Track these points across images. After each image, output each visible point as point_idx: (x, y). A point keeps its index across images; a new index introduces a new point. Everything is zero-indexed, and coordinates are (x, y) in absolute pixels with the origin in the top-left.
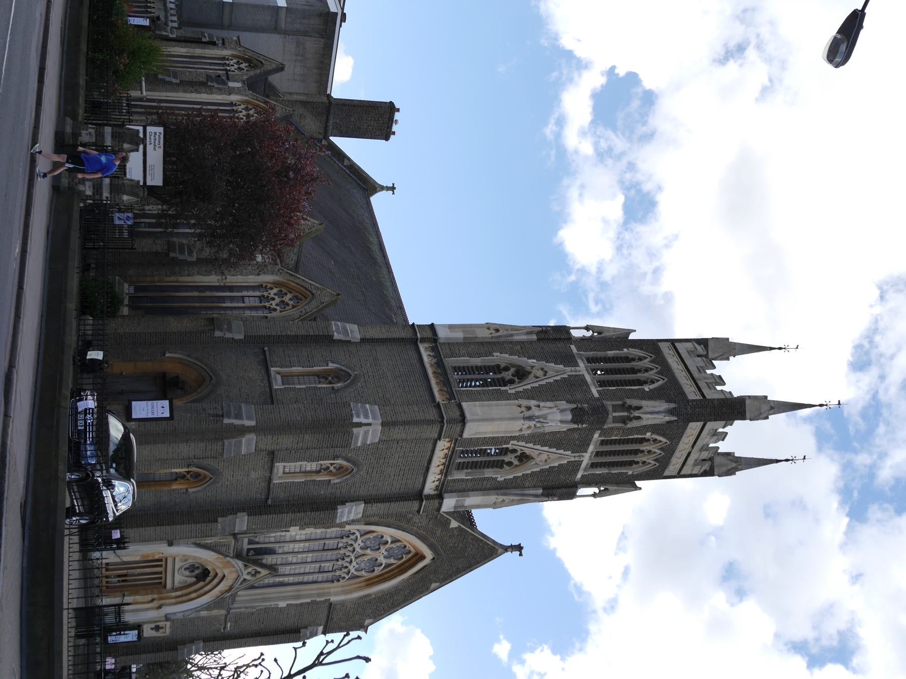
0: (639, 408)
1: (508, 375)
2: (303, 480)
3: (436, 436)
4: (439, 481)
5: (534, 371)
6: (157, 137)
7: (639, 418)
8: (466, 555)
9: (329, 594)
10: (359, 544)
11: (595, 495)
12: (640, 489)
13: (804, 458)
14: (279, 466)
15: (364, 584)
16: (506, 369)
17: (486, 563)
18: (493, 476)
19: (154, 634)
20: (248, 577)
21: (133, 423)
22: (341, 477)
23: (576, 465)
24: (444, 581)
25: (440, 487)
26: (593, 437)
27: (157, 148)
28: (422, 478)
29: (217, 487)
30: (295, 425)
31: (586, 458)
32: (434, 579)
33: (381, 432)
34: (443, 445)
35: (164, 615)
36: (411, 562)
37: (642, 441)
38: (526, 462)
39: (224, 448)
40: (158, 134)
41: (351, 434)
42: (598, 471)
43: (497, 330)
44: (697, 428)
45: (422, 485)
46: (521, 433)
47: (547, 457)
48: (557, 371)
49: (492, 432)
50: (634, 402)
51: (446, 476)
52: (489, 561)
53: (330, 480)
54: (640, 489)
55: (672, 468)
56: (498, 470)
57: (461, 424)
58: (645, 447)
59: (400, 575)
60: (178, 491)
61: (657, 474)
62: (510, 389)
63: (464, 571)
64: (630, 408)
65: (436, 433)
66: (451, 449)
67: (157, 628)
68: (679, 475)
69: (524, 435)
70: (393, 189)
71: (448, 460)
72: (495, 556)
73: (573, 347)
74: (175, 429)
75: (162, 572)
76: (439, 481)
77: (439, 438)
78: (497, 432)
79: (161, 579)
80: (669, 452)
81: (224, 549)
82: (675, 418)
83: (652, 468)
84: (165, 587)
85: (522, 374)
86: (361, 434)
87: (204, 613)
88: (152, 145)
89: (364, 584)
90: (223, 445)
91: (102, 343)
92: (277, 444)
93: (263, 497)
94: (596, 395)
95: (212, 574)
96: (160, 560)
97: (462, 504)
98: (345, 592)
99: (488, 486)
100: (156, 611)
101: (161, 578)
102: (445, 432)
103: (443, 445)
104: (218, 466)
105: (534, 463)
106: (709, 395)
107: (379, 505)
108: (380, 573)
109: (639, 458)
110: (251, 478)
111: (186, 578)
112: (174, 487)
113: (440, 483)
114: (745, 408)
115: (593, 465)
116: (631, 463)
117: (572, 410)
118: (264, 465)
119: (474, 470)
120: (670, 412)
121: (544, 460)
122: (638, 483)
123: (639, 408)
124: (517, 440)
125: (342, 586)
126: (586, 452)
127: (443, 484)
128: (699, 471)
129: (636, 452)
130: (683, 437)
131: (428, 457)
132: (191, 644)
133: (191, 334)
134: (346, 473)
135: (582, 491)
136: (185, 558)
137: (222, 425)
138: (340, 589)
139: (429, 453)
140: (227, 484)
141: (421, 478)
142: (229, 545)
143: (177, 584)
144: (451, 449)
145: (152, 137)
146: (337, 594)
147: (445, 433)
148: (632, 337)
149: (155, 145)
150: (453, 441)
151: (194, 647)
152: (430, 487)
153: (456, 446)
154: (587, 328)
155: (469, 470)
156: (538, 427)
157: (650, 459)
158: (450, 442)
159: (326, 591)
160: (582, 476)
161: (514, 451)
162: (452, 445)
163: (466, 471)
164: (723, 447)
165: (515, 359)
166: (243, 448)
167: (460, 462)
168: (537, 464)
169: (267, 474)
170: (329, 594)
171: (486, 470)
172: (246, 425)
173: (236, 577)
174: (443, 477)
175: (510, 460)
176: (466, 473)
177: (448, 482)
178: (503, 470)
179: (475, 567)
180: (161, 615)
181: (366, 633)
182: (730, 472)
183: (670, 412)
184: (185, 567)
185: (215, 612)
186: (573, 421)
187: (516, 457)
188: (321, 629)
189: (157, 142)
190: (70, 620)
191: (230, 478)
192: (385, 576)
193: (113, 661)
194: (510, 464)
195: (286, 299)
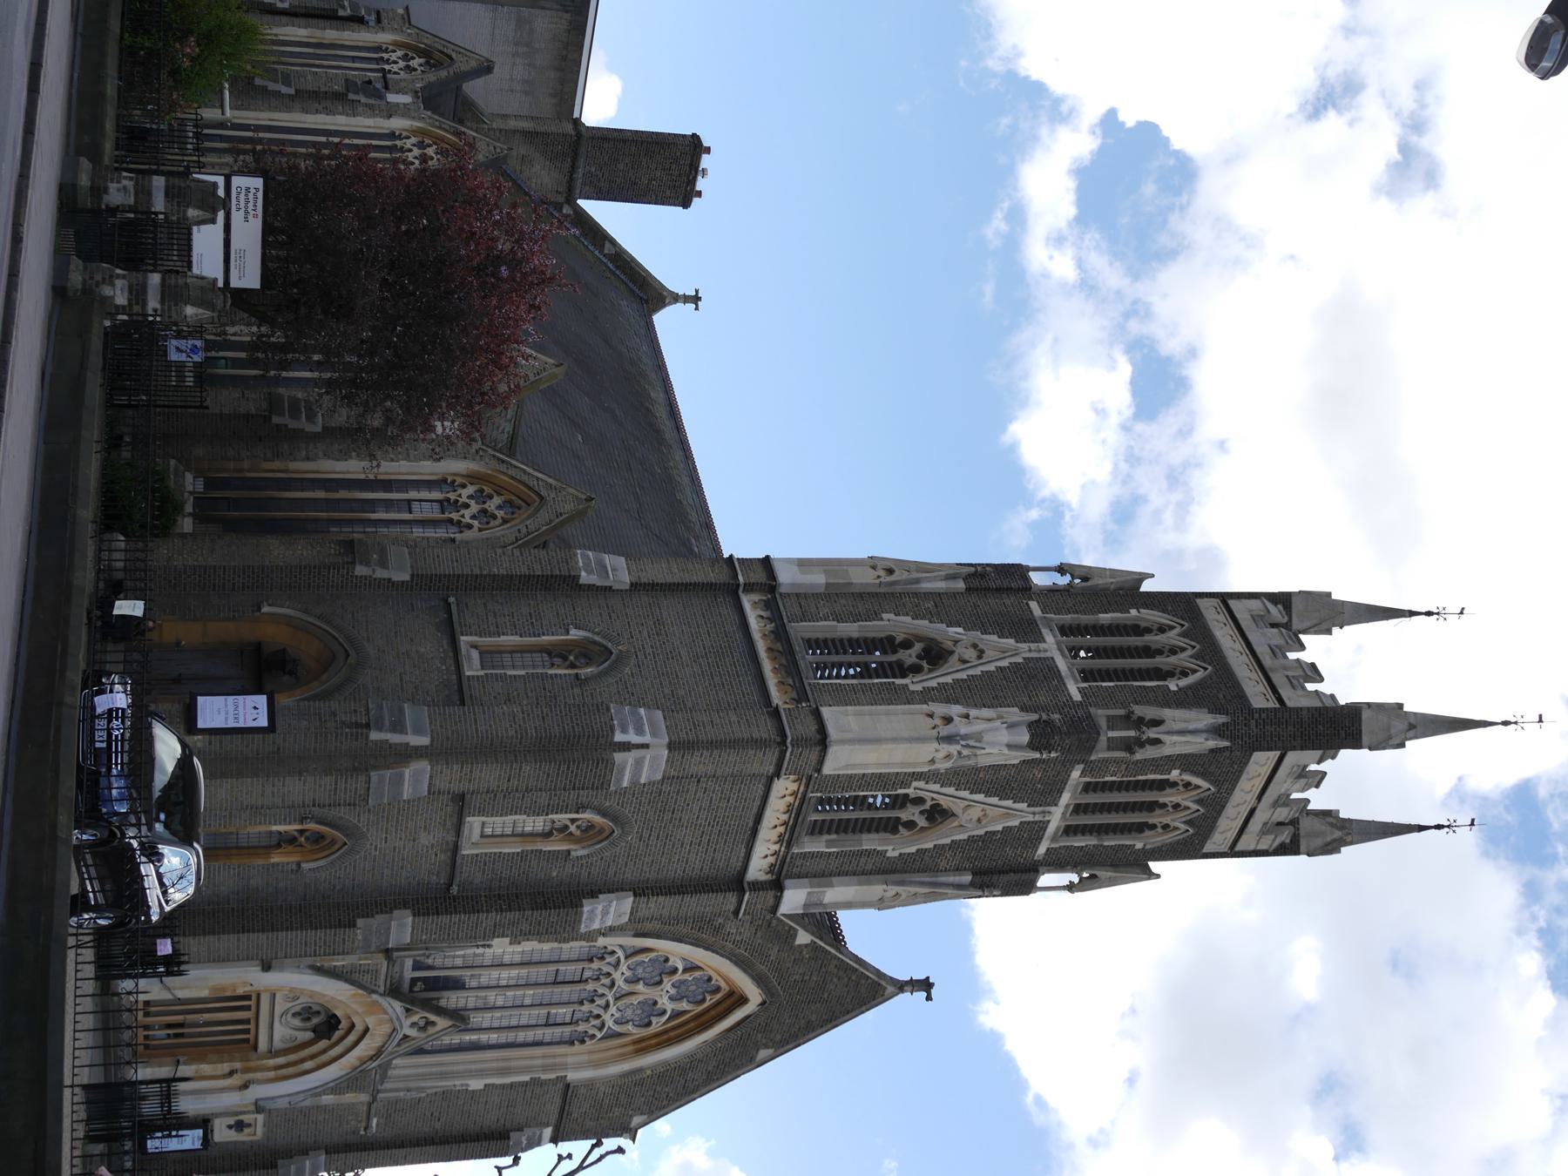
0: (1157, 723)
1: (909, 657)
3: (771, 769)
5: (959, 650)
6: (251, 196)
7: (1157, 742)
9: (565, 1067)
11: (1071, 888)
12: (1158, 876)
13: (1541, 721)
14: (474, 823)
16: (907, 644)
19: (233, 1136)
20: (413, 1033)
21: (200, 737)
23: (1035, 831)
27: (250, 218)
28: (743, 850)
31: (1056, 817)
32: (764, 1041)
33: (667, 761)
34: (784, 788)
35: (254, 1101)
36: (720, 1008)
38: (941, 823)
39: (369, 788)
40: (253, 191)
42: (1079, 842)
43: (890, 571)
44: (1269, 762)
46: (933, 767)
48: (1002, 651)
49: (879, 765)
50: (1150, 712)
53: (569, 852)
54: (1158, 876)
55: (1219, 839)
56: (888, 835)
57: (818, 748)
58: (1168, 797)
59: (699, 1032)
61: (1190, 848)
62: (914, 684)
64: (1140, 723)
65: (770, 764)
67: (240, 1126)
68: (1233, 852)
70: (695, 299)
72: (880, 1000)
73: (1034, 605)
74: (279, 749)
77: (777, 774)
78: (888, 765)
79: (250, 1000)
80: (1214, 807)
82: (1226, 744)
83: (1182, 837)
84: (255, 1048)
85: (935, 655)
86: (629, 764)
87: (327, 1099)
88: (242, 212)
94: (1077, 696)
95: (344, 1025)
98: (596, 1065)
99: (869, 867)
101: (247, 1031)
103: (784, 788)
104: (359, 821)
105: (956, 824)
106: (1292, 699)
107: (661, 899)
109: (1156, 818)
111: (293, 1032)
116: (1140, 828)
117: (1030, 725)
119: (843, 836)
120: (1218, 731)
122: (1154, 866)
123: (1157, 723)
126: (1056, 805)
127: (783, 862)
128: (1271, 846)
129: (1152, 806)
131: (755, 810)
134: (600, 838)
135: (1045, 879)
136: (294, 995)
138: (585, 1058)
139: (757, 803)
143: (277, 1044)
145: (242, 197)
146: (579, 1067)
148: (1147, 587)
149: (247, 212)
151: (308, 1162)
152: (758, 868)
153: (809, 790)
154: (1061, 569)
155: (834, 836)
159: (558, 1060)
161: (919, 801)
163: (826, 837)
164: (1318, 799)
165: (923, 626)
169: (451, 838)
170: (565, 1067)
171: (865, 836)
173: (390, 1031)
174: (783, 849)
175: (912, 818)
177: (792, 858)
178: (897, 836)
179: (841, 1020)
182: (1331, 848)
183: (1218, 731)
185: (349, 1097)
186: (1032, 746)
187: (922, 812)
188: (548, 1132)
189: (251, 205)
192: (672, 1034)
194: (910, 825)
195: (492, 505)
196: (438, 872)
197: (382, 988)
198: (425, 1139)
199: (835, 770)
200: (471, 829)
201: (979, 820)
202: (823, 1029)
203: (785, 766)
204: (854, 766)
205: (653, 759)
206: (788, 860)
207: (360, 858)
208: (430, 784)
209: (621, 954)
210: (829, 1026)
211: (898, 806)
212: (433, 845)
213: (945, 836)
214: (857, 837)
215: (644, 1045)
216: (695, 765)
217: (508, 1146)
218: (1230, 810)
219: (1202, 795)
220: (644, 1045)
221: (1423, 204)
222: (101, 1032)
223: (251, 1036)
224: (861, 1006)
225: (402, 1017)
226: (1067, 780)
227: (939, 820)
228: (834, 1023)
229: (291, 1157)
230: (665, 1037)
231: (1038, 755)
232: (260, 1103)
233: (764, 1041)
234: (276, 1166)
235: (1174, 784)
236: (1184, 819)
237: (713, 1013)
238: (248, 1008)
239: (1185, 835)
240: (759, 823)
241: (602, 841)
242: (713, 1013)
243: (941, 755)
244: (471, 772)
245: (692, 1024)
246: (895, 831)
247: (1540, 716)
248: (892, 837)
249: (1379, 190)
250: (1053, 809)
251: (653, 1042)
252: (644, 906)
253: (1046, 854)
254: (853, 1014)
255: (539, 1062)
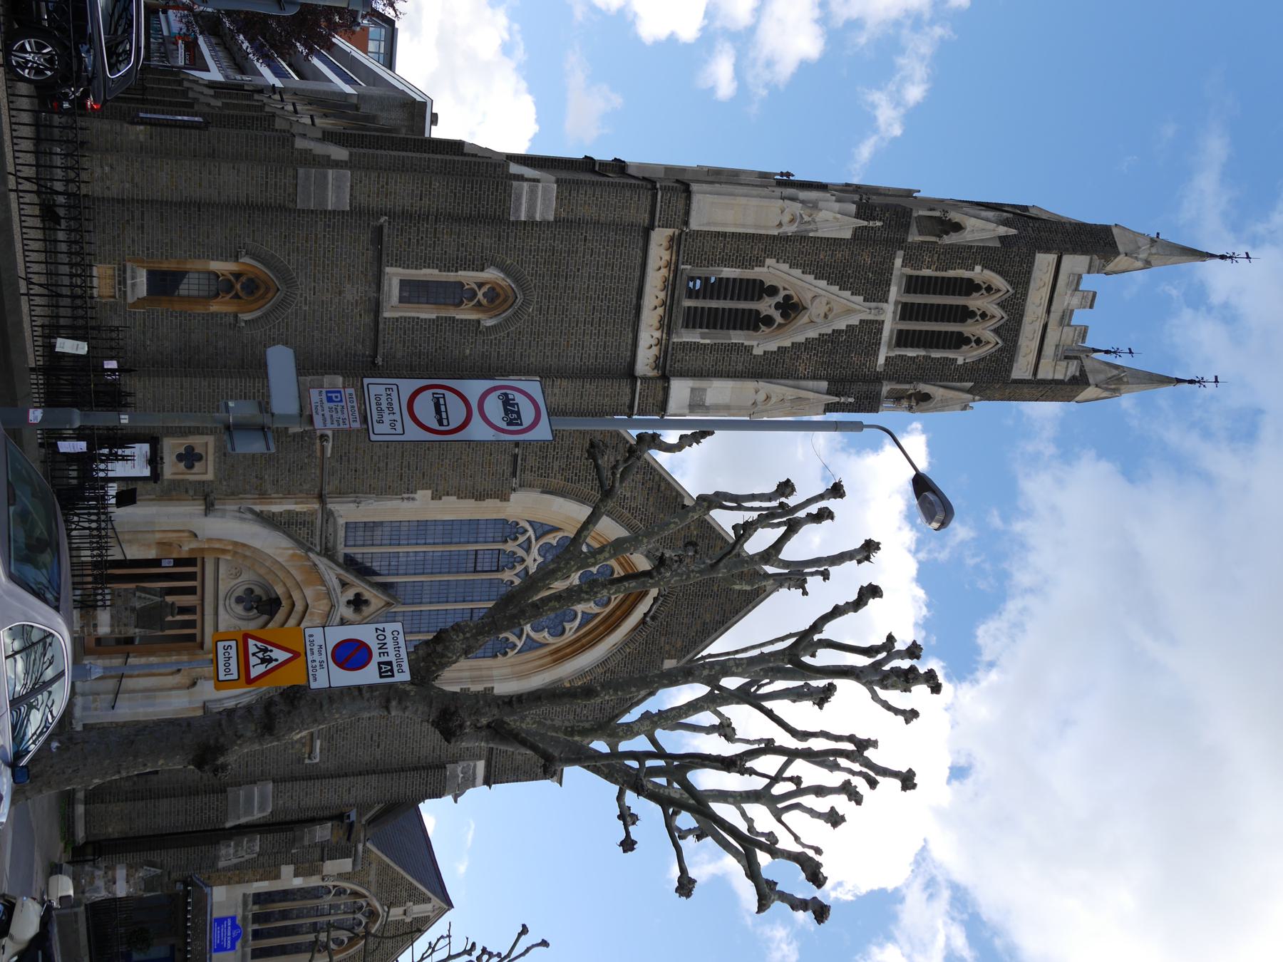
1: (766, 306)
2: (434, 316)
4: (659, 346)
8: (715, 588)
9: (490, 678)
10: (535, 560)
13: (1216, 381)
14: (394, 275)
15: (549, 659)
17: (750, 611)
18: (746, 343)
21: (142, 127)
22: (496, 316)
24: (684, 656)
25: (661, 359)
26: (893, 264)
28: (631, 335)
29: (287, 318)
30: (414, 167)
31: (888, 315)
32: (667, 648)
33: (557, 198)
34: (660, 237)
35: (201, 704)
36: (624, 607)
37: (970, 287)
38: (795, 318)
41: (507, 191)
44: (1050, 268)
45: (632, 351)
46: (781, 230)
47: (827, 308)
49: (736, 225)
51: (669, 334)
52: (754, 607)
53: (478, 321)
56: (751, 332)
57: (684, 195)
60: (221, 318)
63: (716, 630)
66: (672, 266)
69: (786, 233)
71: (669, 293)
72: (762, 596)
74: (214, 150)
75: (195, 607)
76: (659, 346)
77: (651, 227)
78: (743, 226)
79: (195, 627)
80: (1015, 307)
81: (304, 532)
82: (1013, 232)
83: (994, 350)
84: (202, 646)
86: (525, 193)
89: (549, 659)
90: (296, 177)
91: (78, 237)
92: (387, 195)
93: (367, 353)
95: (285, 604)
96: (190, 562)
97: (701, 399)
99: (740, 367)
100: (187, 691)
101: (191, 624)
102: (661, 211)
103: (659, 253)
104: (289, 263)
105: (805, 319)
107: (565, 383)
108: (574, 637)
109: (968, 329)
110: (345, 301)
111: (239, 623)
112: (214, 308)
113: (660, 349)
114: (1113, 238)
115: (903, 339)
116: (959, 341)
118: (366, 269)
121: (823, 315)
124: (775, 257)
125: (513, 665)
126: (887, 301)
128: (1065, 375)
129: (964, 314)
130: (1030, 291)
132: (253, 785)
133: (229, 120)
136: (239, 550)
137: (292, 153)
138: (508, 670)
139: (637, 274)
140: (305, 311)
141: (628, 334)
142: (312, 522)
144: (672, 266)
146: (504, 679)
147: (660, 214)
150: (675, 248)
151: (256, 789)
153: (680, 262)
156: (806, 222)
157: (984, 331)
158: (660, 331)
159: (484, 673)
160: (886, 360)
161: (773, 291)
162: (674, 258)
166: (330, 194)
167: (689, 308)
168: (812, 322)
169: (373, 295)
170: (490, 678)
171: (732, 332)
172: (333, 158)
173: (327, 609)
174: (664, 336)
176: (701, 333)
179: (732, 621)
180: (197, 705)
181: (561, 785)
184: (237, 594)
188: (481, 766)
190: (38, 358)
191: (310, 297)
192: (584, 641)
193: (122, 421)
194: (768, 321)
196: (364, 340)
197: (318, 549)
198: (367, 771)
199: (700, 225)
200: (390, 285)
201: (826, 316)
202: (718, 633)
203: (658, 215)
204: (715, 224)
205: (544, 189)
206: (670, 349)
207: (292, 313)
208: (351, 195)
209: (531, 533)
210: (722, 629)
211: (756, 298)
212: (357, 301)
213: (802, 332)
214: (725, 332)
215: (560, 654)
216: (581, 206)
217: (445, 777)
218: (1023, 342)
219: (1003, 298)
220: (560, 654)
221: (845, 884)
222: (33, 128)
223: (197, 631)
224: (747, 605)
225: (339, 590)
226: (892, 269)
227: (793, 315)
228: (726, 625)
229: (240, 785)
230: (579, 644)
231: (865, 223)
232: (209, 705)
233: (667, 648)
234: (225, 791)
235: (977, 288)
236: (992, 328)
237: (618, 613)
238: (192, 591)
239: (1008, 295)
240: (641, 298)
241: (507, 310)
242: (618, 613)
243: (786, 218)
244: (387, 184)
245: (601, 628)
246: (756, 328)
247: (1216, 377)
248: (755, 334)
249: (881, 596)
250: (884, 305)
251: (568, 650)
252: (550, 390)
253: (885, 365)
254: (742, 613)
255: (467, 674)
